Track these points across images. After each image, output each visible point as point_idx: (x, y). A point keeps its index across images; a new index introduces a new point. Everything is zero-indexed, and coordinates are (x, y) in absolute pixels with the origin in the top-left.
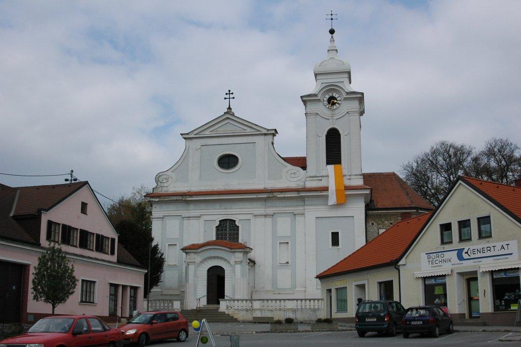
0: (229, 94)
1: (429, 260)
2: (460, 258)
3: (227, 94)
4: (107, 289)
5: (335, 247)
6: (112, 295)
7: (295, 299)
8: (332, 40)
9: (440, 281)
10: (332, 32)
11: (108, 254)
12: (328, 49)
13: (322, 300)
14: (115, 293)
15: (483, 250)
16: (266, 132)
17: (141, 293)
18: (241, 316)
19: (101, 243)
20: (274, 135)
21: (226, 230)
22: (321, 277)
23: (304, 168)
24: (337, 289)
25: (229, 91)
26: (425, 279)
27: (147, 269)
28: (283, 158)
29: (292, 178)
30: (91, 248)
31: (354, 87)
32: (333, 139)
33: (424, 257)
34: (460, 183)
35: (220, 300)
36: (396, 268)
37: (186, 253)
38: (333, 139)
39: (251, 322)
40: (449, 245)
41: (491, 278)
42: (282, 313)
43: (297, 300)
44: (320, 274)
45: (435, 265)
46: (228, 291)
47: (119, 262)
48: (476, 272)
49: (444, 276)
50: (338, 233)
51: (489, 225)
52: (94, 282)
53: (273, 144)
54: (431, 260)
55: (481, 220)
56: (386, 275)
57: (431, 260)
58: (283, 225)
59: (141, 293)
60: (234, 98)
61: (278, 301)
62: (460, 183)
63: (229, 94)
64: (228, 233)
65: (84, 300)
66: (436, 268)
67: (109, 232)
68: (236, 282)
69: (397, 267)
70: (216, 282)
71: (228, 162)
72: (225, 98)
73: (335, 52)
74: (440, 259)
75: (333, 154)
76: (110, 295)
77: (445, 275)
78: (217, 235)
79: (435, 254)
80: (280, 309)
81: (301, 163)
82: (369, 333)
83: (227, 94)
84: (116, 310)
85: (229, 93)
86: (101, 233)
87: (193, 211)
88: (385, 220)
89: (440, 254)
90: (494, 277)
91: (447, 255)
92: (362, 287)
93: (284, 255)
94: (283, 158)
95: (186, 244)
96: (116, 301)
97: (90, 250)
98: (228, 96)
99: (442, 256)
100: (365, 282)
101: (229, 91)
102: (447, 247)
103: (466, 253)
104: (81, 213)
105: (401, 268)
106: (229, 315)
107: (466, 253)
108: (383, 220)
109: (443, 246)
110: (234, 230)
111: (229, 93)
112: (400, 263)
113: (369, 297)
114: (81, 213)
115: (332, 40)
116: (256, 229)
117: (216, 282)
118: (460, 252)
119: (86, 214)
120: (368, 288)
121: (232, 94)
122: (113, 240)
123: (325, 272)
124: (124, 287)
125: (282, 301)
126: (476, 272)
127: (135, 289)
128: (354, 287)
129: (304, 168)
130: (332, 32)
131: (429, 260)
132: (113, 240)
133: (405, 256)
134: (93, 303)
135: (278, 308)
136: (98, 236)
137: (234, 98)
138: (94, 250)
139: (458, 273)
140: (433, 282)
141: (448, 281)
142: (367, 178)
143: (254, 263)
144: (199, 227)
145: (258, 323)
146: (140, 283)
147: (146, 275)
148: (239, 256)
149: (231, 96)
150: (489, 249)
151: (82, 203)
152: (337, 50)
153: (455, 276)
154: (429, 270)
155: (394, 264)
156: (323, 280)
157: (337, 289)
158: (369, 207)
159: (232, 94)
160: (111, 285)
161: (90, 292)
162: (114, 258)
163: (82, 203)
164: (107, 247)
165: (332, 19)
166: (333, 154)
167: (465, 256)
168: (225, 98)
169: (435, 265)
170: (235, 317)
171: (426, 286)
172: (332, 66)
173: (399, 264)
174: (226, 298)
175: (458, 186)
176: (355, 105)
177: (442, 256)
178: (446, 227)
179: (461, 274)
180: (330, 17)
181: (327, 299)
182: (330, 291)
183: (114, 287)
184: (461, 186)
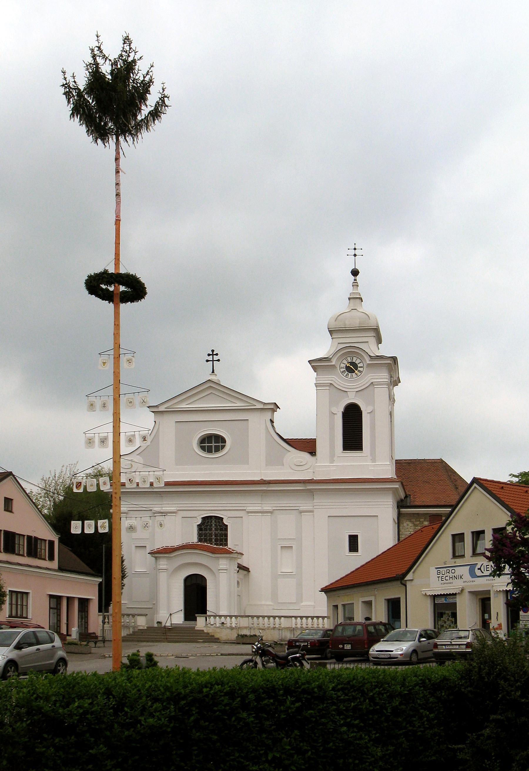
0: (213, 355)
1: (439, 576)
2: (473, 574)
3: (209, 355)
4: (46, 602)
5: (354, 554)
6: (52, 608)
7: (293, 617)
8: (355, 284)
9: (450, 600)
10: (355, 273)
11: (45, 559)
12: (349, 296)
13: (328, 617)
14: (57, 606)
15: (487, 568)
16: (261, 406)
17: (94, 607)
18: (224, 635)
19: (33, 547)
20: (273, 411)
21: (211, 530)
22: (326, 590)
23: (313, 453)
24: (344, 605)
25: (213, 351)
26: (434, 597)
27: (101, 576)
28: (285, 440)
29: (296, 466)
30: (21, 553)
31: (385, 350)
32: (352, 417)
33: (433, 571)
34: (475, 487)
35: (196, 615)
36: (402, 584)
37: (156, 558)
38: (352, 417)
39: (234, 643)
40: (461, 559)
41: (433, 604)
42: (276, 632)
43: (296, 617)
44: (326, 587)
45: (445, 581)
46: (210, 606)
47: (61, 569)
48: (489, 592)
49: (455, 594)
50: (357, 536)
51: (463, 543)
52: (27, 593)
53: (272, 421)
54: (441, 575)
55: (457, 537)
56: (393, 592)
57: (441, 575)
58: (286, 525)
59: (94, 607)
60: (218, 360)
61: (304, 618)
62: (475, 487)
63: (213, 355)
64: (213, 533)
65: (14, 614)
66: (446, 585)
67: (45, 533)
68: (218, 599)
69: (403, 582)
70: (196, 595)
71: (212, 443)
72: (207, 361)
73: (358, 301)
74: (451, 575)
75: (353, 439)
76: (50, 608)
77: (455, 594)
78: (200, 535)
79: (445, 569)
80: (274, 628)
81: (308, 446)
82: (345, 659)
83: (209, 355)
84: (60, 626)
85: (213, 354)
86: (33, 534)
87: (168, 505)
88: (425, 521)
89: (450, 569)
90: (436, 602)
91: (459, 571)
92: (369, 604)
93: (287, 565)
94: (285, 440)
95: (159, 545)
96: (59, 615)
97: (19, 555)
98: (210, 358)
99: (453, 571)
100: (372, 598)
101: (213, 351)
102: (459, 561)
103: (479, 569)
104: (5, 510)
105: (408, 585)
106: (208, 633)
107: (479, 569)
108: (421, 520)
109: (453, 560)
110: (221, 530)
111: (213, 354)
112: (408, 577)
113: (376, 616)
114: (5, 510)
115: (355, 284)
116: (250, 530)
117: (196, 595)
118: (472, 567)
119: (11, 512)
120: (375, 607)
121: (217, 354)
122: (51, 543)
123: (332, 584)
124: (69, 599)
125: (277, 618)
126: (489, 592)
127: (84, 603)
128: (360, 603)
129: (313, 453)
130: (355, 273)
131: (439, 576)
132: (51, 543)
133: (412, 570)
134: (26, 618)
135: (272, 626)
136: (29, 538)
137: (218, 360)
138: (25, 555)
139: (469, 592)
140: (443, 600)
141: (459, 600)
142: (402, 466)
143: (247, 569)
144: (179, 527)
145: (243, 644)
146: (93, 595)
147: (100, 585)
148: (223, 563)
149: (216, 358)
150: (448, 571)
151: (5, 498)
152: (361, 299)
153: (466, 595)
154: (438, 587)
155: (400, 579)
156: (332, 593)
157: (344, 605)
158: (401, 504)
159: (217, 354)
160: (51, 596)
161: (22, 605)
162: (55, 564)
163: (5, 498)
164: (43, 551)
165: (355, 255)
166: (353, 439)
167: (478, 573)
168: (207, 361)
169: (445, 581)
170: (217, 636)
171: (435, 605)
172: (354, 320)
173: (406, 579)
174: (208, 613)
175: (473, 490)
176: (383, 376)
177: (453, 571)
178: (458, 538)
179: (473, 593)
180: (353, 252)
181: (333, 618)
182: (336, 607)
183: (55, 600)
184: (476, 491)
